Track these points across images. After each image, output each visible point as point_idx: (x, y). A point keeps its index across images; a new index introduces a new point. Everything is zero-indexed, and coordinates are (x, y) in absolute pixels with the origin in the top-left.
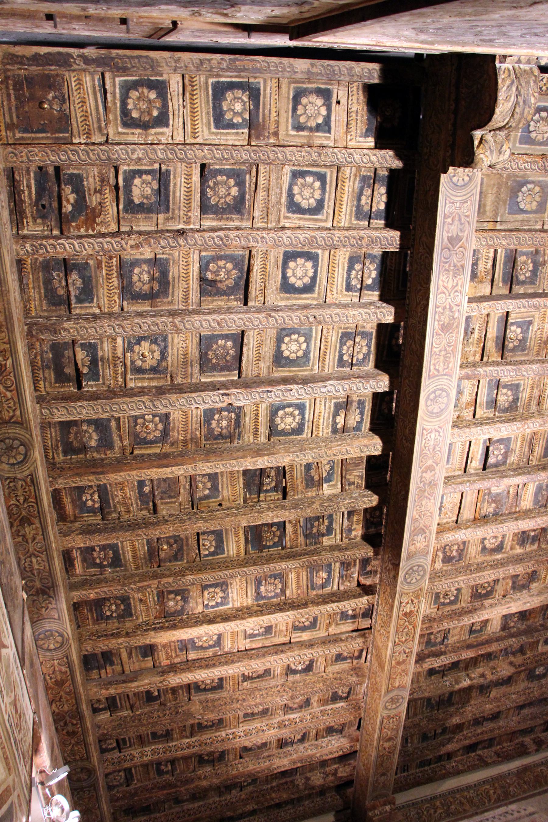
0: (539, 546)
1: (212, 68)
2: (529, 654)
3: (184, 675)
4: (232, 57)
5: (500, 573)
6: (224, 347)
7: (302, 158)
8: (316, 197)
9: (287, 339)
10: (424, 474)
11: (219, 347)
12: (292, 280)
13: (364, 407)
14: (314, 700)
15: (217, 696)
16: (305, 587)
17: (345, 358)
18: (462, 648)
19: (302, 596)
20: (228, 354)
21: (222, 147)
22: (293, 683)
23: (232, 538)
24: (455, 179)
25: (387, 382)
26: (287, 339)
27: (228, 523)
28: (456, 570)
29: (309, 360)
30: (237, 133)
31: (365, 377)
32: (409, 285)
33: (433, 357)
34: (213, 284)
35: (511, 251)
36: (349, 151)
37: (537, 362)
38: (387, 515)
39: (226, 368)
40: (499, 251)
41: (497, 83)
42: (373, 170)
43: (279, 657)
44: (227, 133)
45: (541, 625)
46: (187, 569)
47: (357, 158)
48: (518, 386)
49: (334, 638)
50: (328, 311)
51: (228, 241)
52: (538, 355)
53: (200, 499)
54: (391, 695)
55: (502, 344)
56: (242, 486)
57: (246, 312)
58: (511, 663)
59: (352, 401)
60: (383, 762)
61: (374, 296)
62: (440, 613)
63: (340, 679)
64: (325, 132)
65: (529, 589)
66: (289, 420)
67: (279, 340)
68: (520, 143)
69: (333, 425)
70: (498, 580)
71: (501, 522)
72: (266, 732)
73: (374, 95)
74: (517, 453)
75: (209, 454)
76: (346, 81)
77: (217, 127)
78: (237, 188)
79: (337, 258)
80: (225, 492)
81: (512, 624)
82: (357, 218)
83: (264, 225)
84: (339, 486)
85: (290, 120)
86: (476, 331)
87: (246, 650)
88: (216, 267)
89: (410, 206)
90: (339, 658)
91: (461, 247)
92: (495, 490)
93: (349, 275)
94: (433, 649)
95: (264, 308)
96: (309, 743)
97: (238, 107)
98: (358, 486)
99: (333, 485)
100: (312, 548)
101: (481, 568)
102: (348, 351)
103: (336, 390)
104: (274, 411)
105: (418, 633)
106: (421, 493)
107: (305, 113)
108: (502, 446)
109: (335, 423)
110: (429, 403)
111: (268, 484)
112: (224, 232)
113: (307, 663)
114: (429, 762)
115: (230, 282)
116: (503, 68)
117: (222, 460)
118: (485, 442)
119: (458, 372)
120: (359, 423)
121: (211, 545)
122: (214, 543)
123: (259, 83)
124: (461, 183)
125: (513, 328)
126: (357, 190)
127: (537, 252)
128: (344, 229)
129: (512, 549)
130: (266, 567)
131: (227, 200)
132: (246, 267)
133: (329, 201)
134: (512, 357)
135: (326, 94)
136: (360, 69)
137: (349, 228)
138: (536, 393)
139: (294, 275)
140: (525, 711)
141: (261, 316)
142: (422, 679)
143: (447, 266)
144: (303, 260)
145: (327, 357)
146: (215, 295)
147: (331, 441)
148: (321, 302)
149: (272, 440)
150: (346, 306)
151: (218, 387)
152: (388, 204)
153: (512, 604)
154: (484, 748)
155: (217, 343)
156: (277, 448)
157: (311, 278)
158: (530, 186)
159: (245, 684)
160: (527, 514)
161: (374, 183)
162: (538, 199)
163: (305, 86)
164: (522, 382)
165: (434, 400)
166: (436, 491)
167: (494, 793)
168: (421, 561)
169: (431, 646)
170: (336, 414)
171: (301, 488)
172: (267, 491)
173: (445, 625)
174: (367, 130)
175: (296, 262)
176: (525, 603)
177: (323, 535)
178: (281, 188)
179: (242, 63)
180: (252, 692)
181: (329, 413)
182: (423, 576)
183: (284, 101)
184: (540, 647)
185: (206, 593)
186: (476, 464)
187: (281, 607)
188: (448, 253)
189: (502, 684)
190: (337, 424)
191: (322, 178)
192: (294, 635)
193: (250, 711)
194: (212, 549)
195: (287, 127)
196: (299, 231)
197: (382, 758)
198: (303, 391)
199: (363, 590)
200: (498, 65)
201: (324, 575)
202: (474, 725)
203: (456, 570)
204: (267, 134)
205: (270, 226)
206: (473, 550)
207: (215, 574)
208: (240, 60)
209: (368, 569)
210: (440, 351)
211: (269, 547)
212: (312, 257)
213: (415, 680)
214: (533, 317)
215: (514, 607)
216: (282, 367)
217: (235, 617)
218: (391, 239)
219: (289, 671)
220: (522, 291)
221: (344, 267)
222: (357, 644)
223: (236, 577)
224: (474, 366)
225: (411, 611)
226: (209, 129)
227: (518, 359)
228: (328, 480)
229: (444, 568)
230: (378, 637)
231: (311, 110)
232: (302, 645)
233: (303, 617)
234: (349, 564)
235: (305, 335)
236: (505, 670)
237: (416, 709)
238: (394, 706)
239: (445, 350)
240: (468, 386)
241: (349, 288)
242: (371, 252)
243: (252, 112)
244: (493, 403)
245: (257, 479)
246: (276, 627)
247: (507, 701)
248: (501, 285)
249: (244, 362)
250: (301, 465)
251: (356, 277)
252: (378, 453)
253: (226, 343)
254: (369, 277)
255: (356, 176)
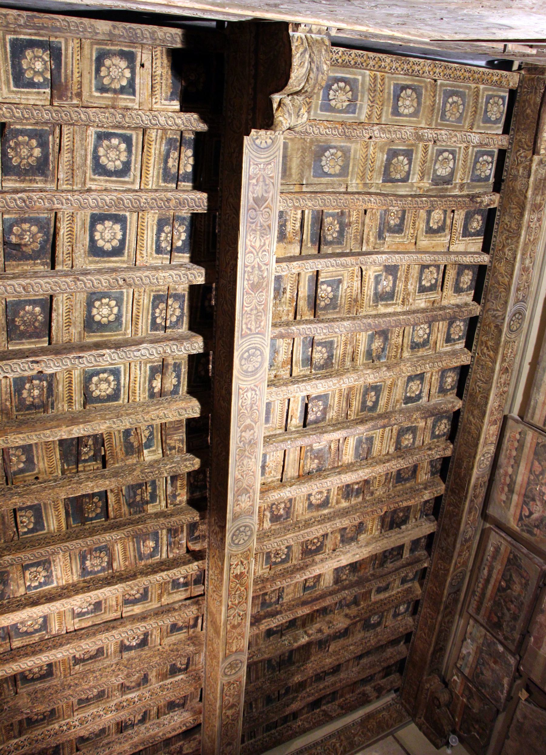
0: (363, 498)
1: (8, 23)
2: (363, 604)
3: (7, 665)
4: (30, 13)
5: (328, 528)
6: (32, 313)
7: (106, 119)
8: (122, 159)
9: (97, 304)
10: (243, 434)
11: (27, 313)
12: (100, 243)
13: (180, 370)
14: (152, 676)
15: (47, 685)
16: (132, 558)
17: (159, 321)
18: (297, 605)
19: (130, 567)
20: (36, 320)
21: (22, 106)
22: (128, 660)
23: (51, 512)
24: (258, 142)
25: (202, 344)
26: (97, 304)
27: (46, 497)
28: (285, 528)
29: (121, 324)
30: (39, 93)
31: (180, 339)
32: (218, 245)
33: (245, 316)
34: (17, 248)
35: (318, 212)
36: (153, 113)
37: (348, 319)
38: (210, 477)
39: (35, 335)
40: (306, 212)
41: (291, 50)
42: (179, 133)
43: (110, 634)
44: (28, 92)
45: (372, 575)
46: (5, 549)
47: (162, 120)
48: (332, 343)
49: (167, 608)
50: (138, 274)
51: (30, 203)
52: (349, 312)
53: (15, 473)
54: (229, 660)
55: (314, 302)
56: (58, 457)
57: (52, 276)
58: (346, 615)
59: (168, 364)
60: (227, 731)
61: (185, 258)
62: (272, 572)
63: (177, 650)
64: (129, 94)
65: (358, 542)
66: (104, 386)
67: (90, 305)
68: (321, 110)
69: (149, 390)
70: (327, 535)
71: (325, 478)
72: (104, 716)
73: (178, 60)
74: (336, 408)
75: (21, 425)
76: (149, 45)
77: (17, 85)
78: (39, 149)
79: (146, 220)
80: (41, 465)
81: (344, 577)
82: (165, 181)
83: (69, 187)
84: (160, 451)
85: (94, 81)
86: (288, 290)
87: (75, 630)
88: (20, 231)
89: (216, 167)
90: (174, 628)
91: (266, 207)
92: (316, 447)
93: (158, 237)
94: (269, 609)
95: (72, 272)
96: (151, 723)
97: (39, 66)
98: (180, 451)
99: (154, 451)
100: (137, 517)
101: (309, 524)
102: (161, 314)
103: (150, 353)
104: (88, 377)
105: (251, 595)
106: (242, 453)
107: (109, 75)
108: (320, 403)
109: (151, 388)
110: (243, 362)
111: (86, 453)
112: (27, 194)
113: (142, 637)
114: (275, 725)
115: (36, 246)
116: (296, 37)
117: (35, 431)
118: (303, 400)
119: (270, 332)
120: (177, 386)
121: (30, 522)
122: (32, 519)
123: (60, 43)
124: (264, 145)
125: (324, 287)
126: (163, 152)
127: (342, 213)
128: (151, 191)
129: (338, 502)
130: (89, 540)
131: (30, 161)
132: (52, 230)
133: (135, 163)
134: (324, 315)
135: (130, 57)
136: (162, 34)
137: (156, 191)
138: (350, 349)
139: (102, 238)
140: (364, 661)
141: (69, 280)
142: (261, 642)
143: (253, 226)
144: (111, 223)
145: (140, 321)
146: (20, 260)
147: (148, 406)
148: (131, 265)
149: (88, 407)
150: (156, 268)
151: (27, 354)
152: (195, 167)
153: (342, 557)
154: (328, 702)
155: (24, 309)
156: (93, 415)
157: (119, 240)
158: (332, 151)
159: (77, 667)
160: (349, 468)
161: (181, 146)
162: (340, 163)
163: (108, 48)
164: (336, 339)
165: (248, 359)
166: (256, 450)
167: (341, 745)
168: (248, 521)
169: (265, 606)
170: (152, 378)
171: (121, 455)
172: (85, 461)
173: (279, 584)
174: (172, 94)
175: (103, 224)
176: (354, 555)
177: (147, 503)
178: (86, 150)
179: (41, 21)
180: (84, 675)
181: (145, 378)
182: (250, 536)
183: (86, 62)
184: (372, 597)
185: (27, 573)
186: (296, 421)
187: (109, 581)
188: (254, 213)
189: (339, 637)
190: (153, 388)
191: (127, 140)
192: (125, 610)
193: (84, 697)
194: (31, 526)
195: (91, 88)
196: (104, 193)
197: (226, 728)
198: (116, 356)
199: (192, 555)
200: (291, 33)
201: (151, 544)
202: (316, 681)
203: (285, 528)
204: (70, 95)
205: (75, 188)
206: (300, 507)
207: (35, 552)
208: (39, 17)
209: (196, 534)
210: (252, 310)
211: (92, 519)
212: (120, 220)
213: (254, 643)
214: (342, 275)
215: (345, 560)
216: (94, 332)
217: (60, 596)
218: (199, 201)
219: (123, 648)
220: (330, 251)
221: (153, 230)
222: (191, 612)
223: (58, 553)
224: (287, 325)
225: (241, 573)
226: (9, 87)
227: (330, 316)
228: (148, 446)
229: (273, 527)
230: (212, 602)
231: (114, 72)
232: (134, 619)
233: (132, 589)
234: (176, 531)
235: (116, 299)
236: (340, 622)
237: (257, 672)
238: (234, 671)
239: (256, 309)
240: (283, 345)
241: (159, 250)
242: (180, 214)
243: (54, 72)
244: (309, 361)
245: (74, 449)
246: (105, 603)
247: (346, 654)
248: (309, 245)
249: (53, 328)
250: (119, 431)
251: (166, 239)
252: (197, 415)
253: (34, 308)
254: (179, 239)
255: (162, 138)
